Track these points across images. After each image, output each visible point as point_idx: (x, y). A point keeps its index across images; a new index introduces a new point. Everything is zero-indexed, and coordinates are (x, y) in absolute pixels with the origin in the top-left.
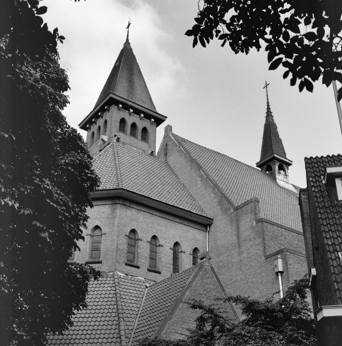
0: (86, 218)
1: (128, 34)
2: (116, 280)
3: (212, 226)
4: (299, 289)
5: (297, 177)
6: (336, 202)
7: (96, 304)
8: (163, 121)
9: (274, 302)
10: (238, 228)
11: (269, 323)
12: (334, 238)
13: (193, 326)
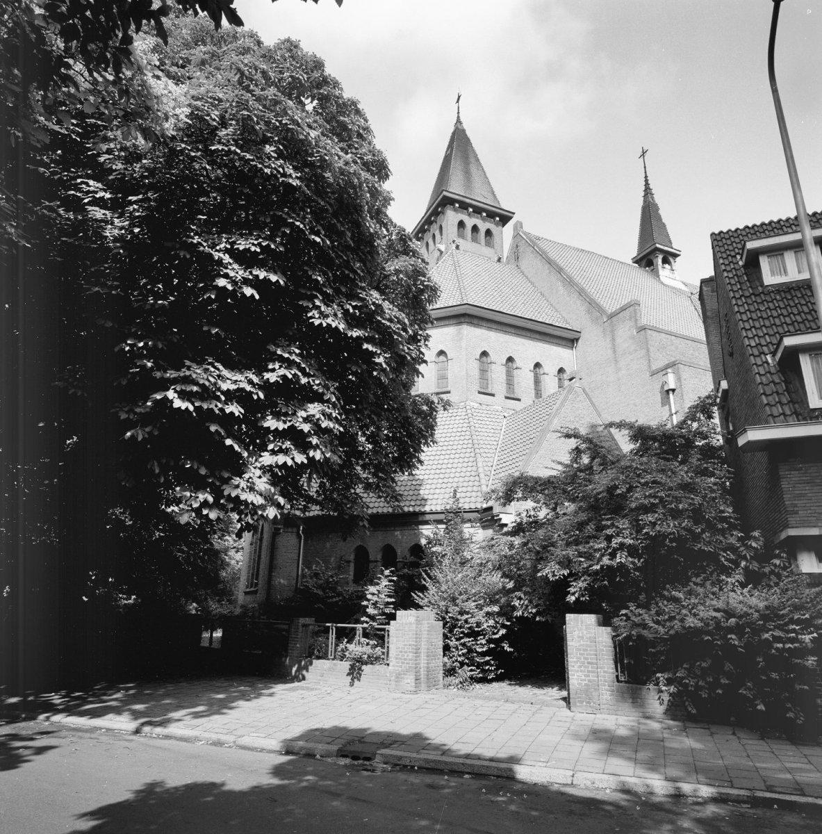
0: (427, 338)
2: (469, 411)
3: (580, 341)
4: (703, 408)
5: (695, 264)
6: (760, 288)
7: (447, 439)
8: (511, 218)
9: (669, 426)
10: (613, 340)
11: (664, 452)
12: (759, 337)
13: (566, 459)
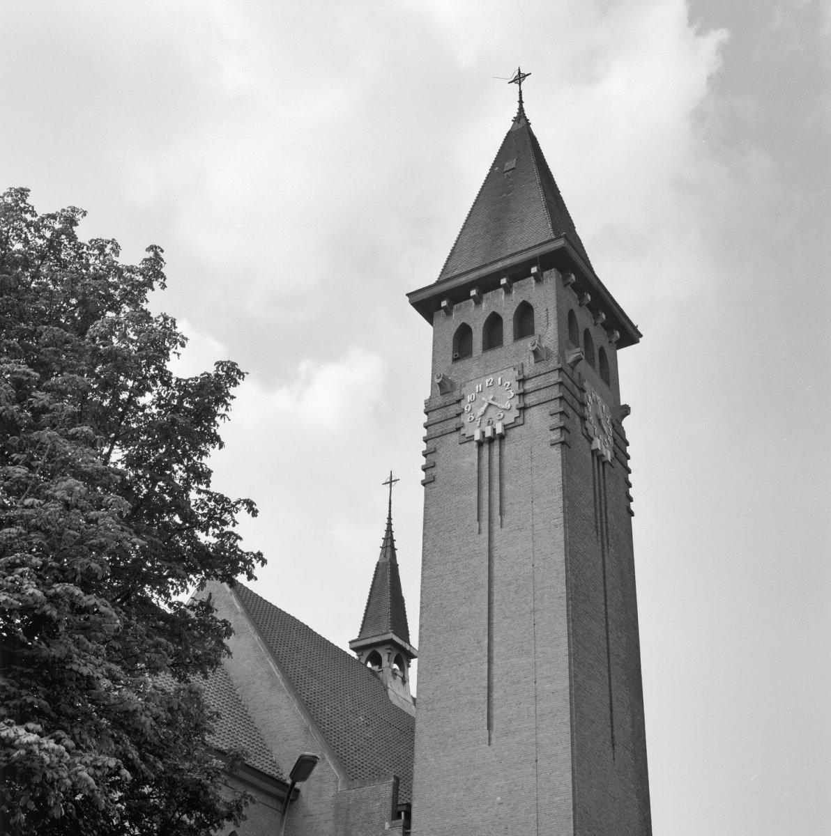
1: (521, 97)
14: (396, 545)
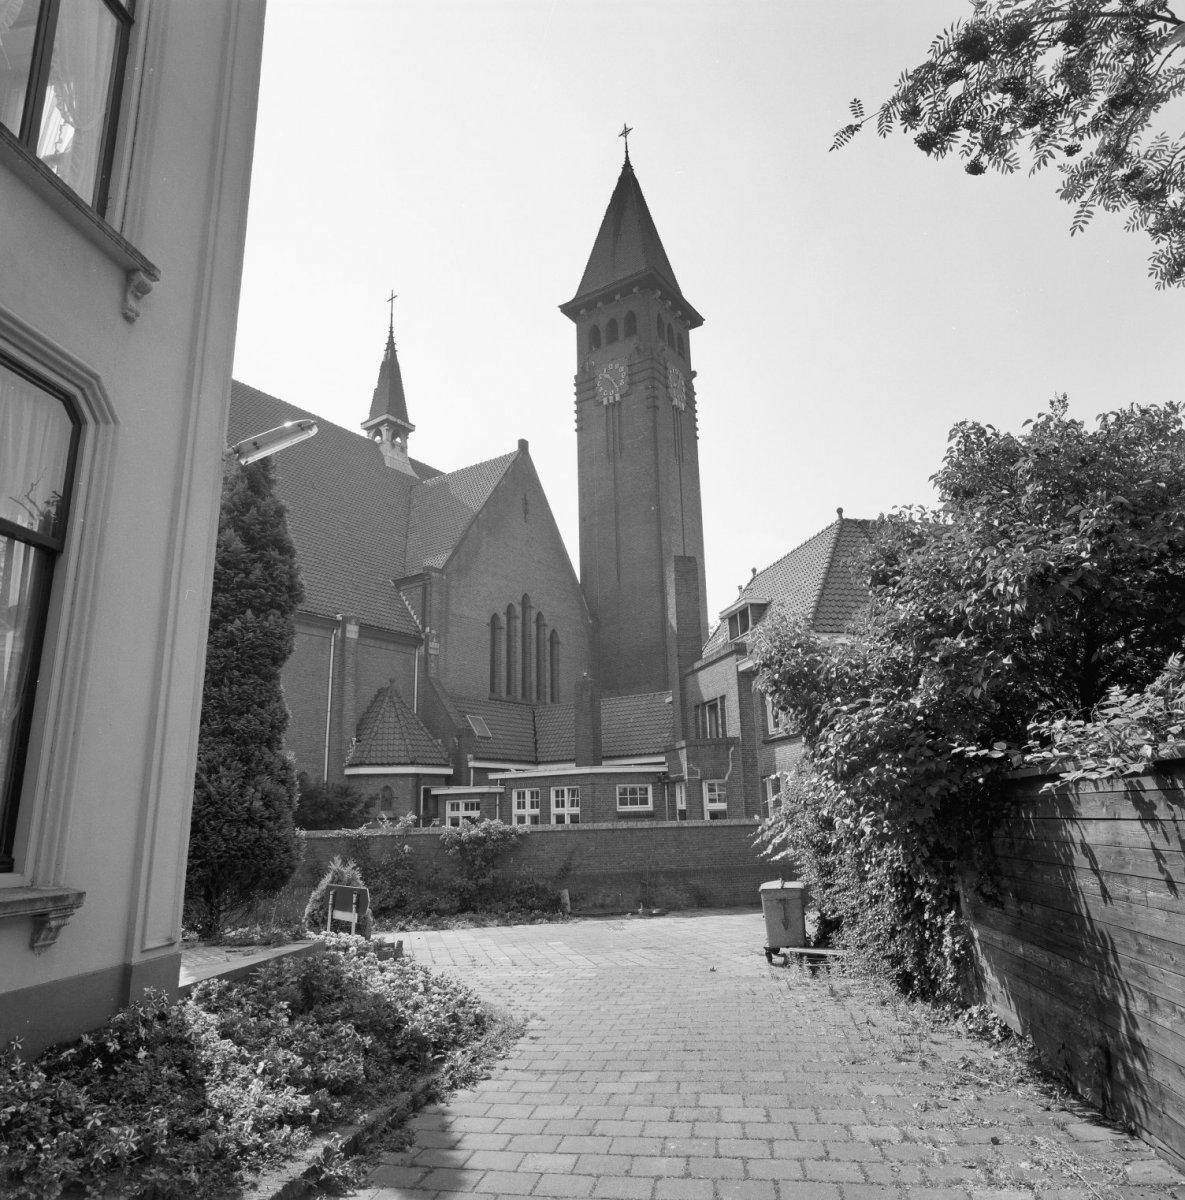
14: (397, 348)
